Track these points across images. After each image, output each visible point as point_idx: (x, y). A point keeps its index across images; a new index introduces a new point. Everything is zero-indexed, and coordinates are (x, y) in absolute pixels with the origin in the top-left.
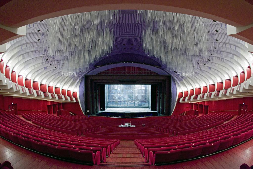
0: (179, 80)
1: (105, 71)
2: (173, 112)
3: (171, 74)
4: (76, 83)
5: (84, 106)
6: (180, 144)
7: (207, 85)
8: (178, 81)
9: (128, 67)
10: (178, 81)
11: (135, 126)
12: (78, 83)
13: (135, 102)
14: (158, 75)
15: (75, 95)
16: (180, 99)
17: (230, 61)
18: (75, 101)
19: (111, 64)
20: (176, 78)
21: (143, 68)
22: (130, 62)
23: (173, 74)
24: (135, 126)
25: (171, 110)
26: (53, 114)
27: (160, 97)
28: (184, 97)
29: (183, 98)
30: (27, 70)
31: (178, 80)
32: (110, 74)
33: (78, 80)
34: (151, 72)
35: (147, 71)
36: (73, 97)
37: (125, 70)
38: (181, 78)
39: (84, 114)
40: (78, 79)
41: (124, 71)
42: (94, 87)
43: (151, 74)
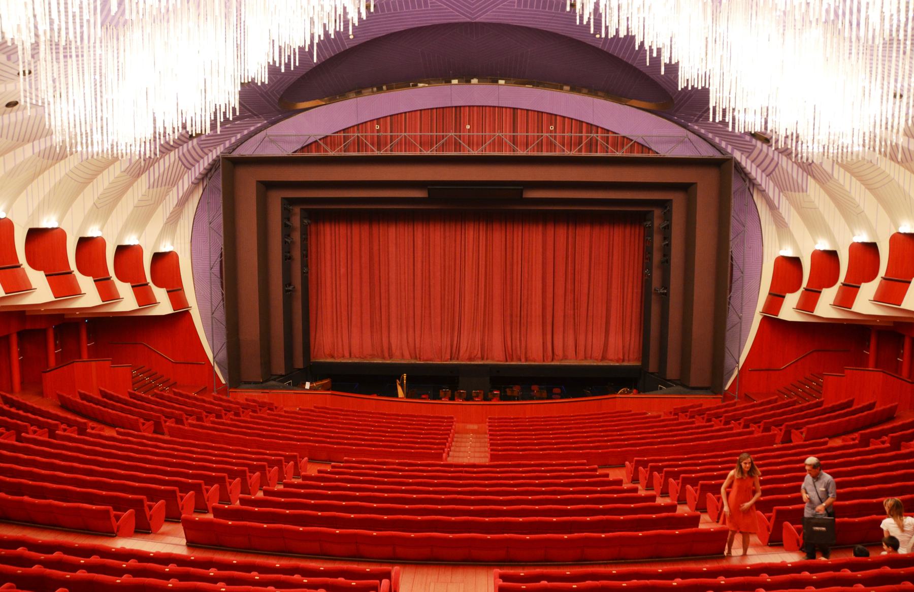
0: (782, 188)
1: (344, 130)
2: (740, 372)
3: (729, 149)
5: (222, 339)
8: (771, 190)
11: (663, 73)
12: (182, 202)
17: (362, 313)
18: (163, 306)
19: (380, 89)
20: (763, 171)
22: (490, 76)
23: (743, 152)
24: (663, 73)
25: (729, 361)
26: (23, 389)
27: (888, 448)
28: (806, 289)
32: (373, 151)
33: (186, 182)
34: (606, 139)
35: (584, 134)
37: (458, 128)
38: (795, 172)
39: (224, 382)
40: (182, 177)
42: (310, 224)
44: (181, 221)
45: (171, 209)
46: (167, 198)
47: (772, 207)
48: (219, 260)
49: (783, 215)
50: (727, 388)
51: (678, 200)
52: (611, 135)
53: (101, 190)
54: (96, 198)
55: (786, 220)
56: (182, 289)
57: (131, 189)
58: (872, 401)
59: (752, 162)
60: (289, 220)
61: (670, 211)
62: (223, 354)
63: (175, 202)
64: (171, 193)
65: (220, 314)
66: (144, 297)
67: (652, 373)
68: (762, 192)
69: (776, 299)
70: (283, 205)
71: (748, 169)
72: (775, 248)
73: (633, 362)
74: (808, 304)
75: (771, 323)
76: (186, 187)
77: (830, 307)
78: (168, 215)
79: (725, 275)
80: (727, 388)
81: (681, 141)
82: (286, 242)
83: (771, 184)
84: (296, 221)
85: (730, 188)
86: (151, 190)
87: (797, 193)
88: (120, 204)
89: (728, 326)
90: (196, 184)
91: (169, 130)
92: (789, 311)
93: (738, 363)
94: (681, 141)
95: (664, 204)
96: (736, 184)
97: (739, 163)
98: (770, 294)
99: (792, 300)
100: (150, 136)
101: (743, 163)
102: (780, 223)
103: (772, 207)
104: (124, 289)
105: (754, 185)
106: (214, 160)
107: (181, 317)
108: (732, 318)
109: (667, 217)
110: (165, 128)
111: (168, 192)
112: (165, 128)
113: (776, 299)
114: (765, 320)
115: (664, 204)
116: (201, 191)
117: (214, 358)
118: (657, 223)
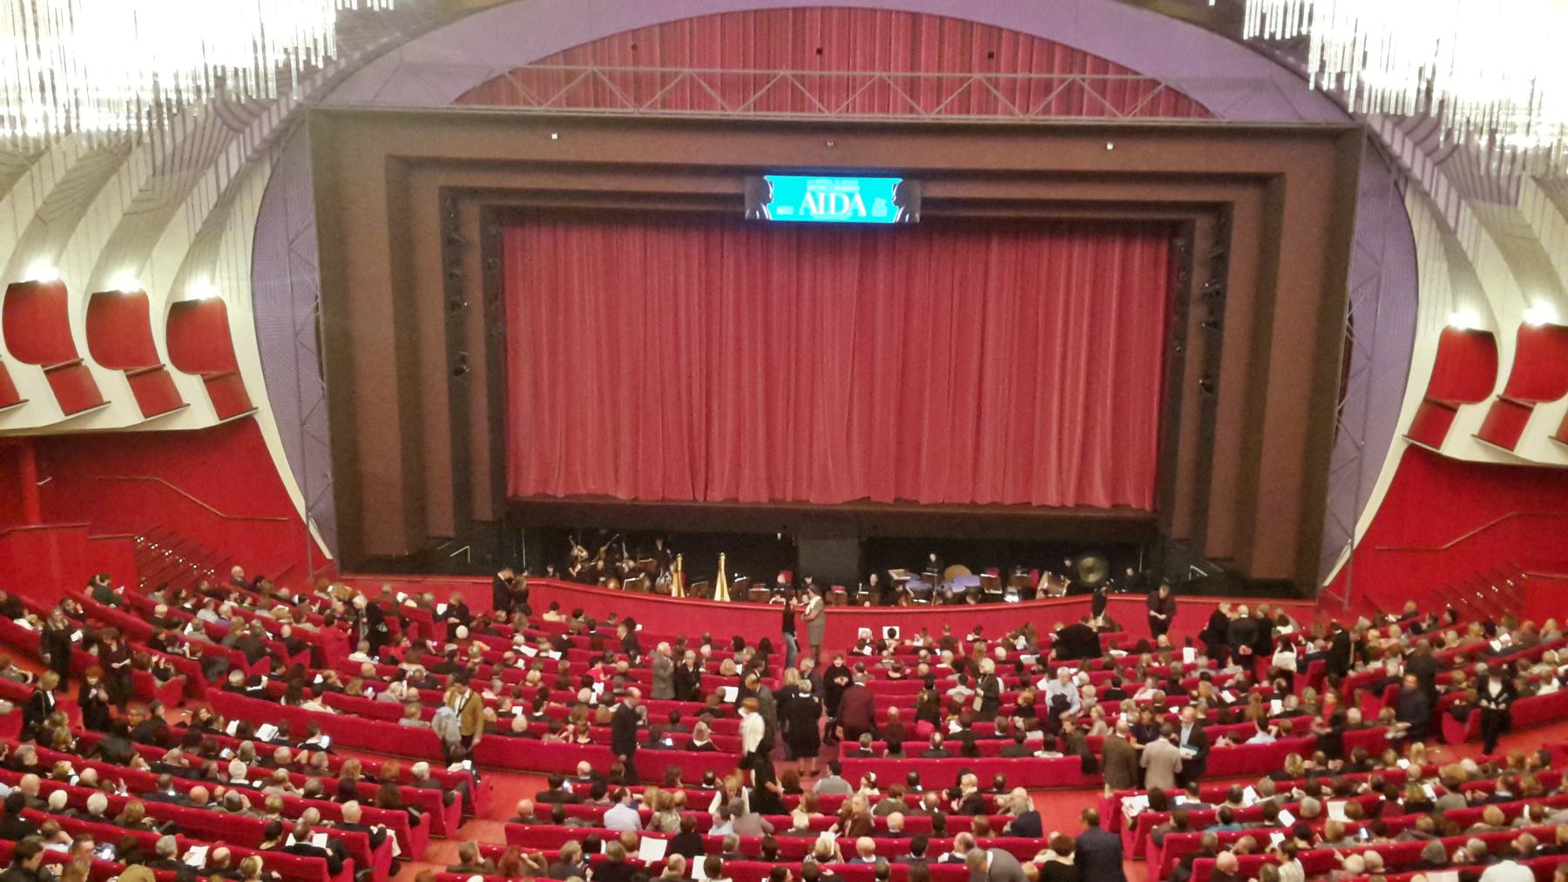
2: (1356, 553)
4: (207, 193)
6: (877, 583)
7: (1491, 317)
9: (835, 15)
10: (1443, 195)
12: (226, 201)
13: (259, 591)
14: (1194, 121)
15: (199, 333)
16: (1526, 411)
18: (197, 410)
21: (1016, 34)
25: (1332, 530)
28: (1503, 400)
29: (1492, 399)
30: (81, 224)
31: (1451, 181)
36: (170, 368)
39: (329, 556)
40: (225, 148)
41: (786, 72)
43: (1102, 113)
44: (228, 235)
45: (205, 214)
46: (195, 190)
47: (1446, 233)
48: (313, 317)
49: (1464, 245)
50: (1327, 582)
51: (1245, 203)
52: (1130, 77)
53: (49, 187)
54: (39, 203)
55: (1470, 256)
56: (237, 373)
57: (114, 178)
58: (1211, 108)
59: (1416, 144)
60: (457, 230)
61: (1229, 219)
62: (327, 504)
63: (213, 199)
64: (202, 181)
65: (320, 424)
66: (154, 393)
67: (1180, 541)
68: (1425, 197)
69: (1435, 418)
70: (442, 198)
71: (1396, 148)
72: (1446, 313)
73: (1137, 500)
74: (1505, 427)
75: (1423, 462)
76: (234, 169)
77: (1546, 439)
78: (199, 226)
79: (1332, 361)
80: (1327, 582)
81: (1257, 85)
82: (451, 276)
83: (1443, 181)
84: (472, 231)
85: (1354, 184)
86: (158, 179)
87: (1488, 205)
88: (92, 207)
89: (1333, 466)
90: (254, 162)
91: (188, 96)
92: (1464, 440)
93: (1352, 536)
94: (1257, 85)
95: (1219, 210)
96: (1367, 177)
97: (1378, 137)
98: (1426, 400)
99: (1470, 418)
100: (148, 97)
101: (1387, 138)
102: (1459, 264)
103: (1446, 233)
104: (112, 384)
105: (1407, 179)
106: (291, 113)
107: (237, 431)
108: (1344, 445)
109: (1221, 236)
110: (178, 91)
111: (195, 182)
112: (178, 91)
113: (1435, 418)
114: (1412, 454)
115: (1219, 210)
116: (268, 172)
117: (308, 509)
118: (1202, 246)
